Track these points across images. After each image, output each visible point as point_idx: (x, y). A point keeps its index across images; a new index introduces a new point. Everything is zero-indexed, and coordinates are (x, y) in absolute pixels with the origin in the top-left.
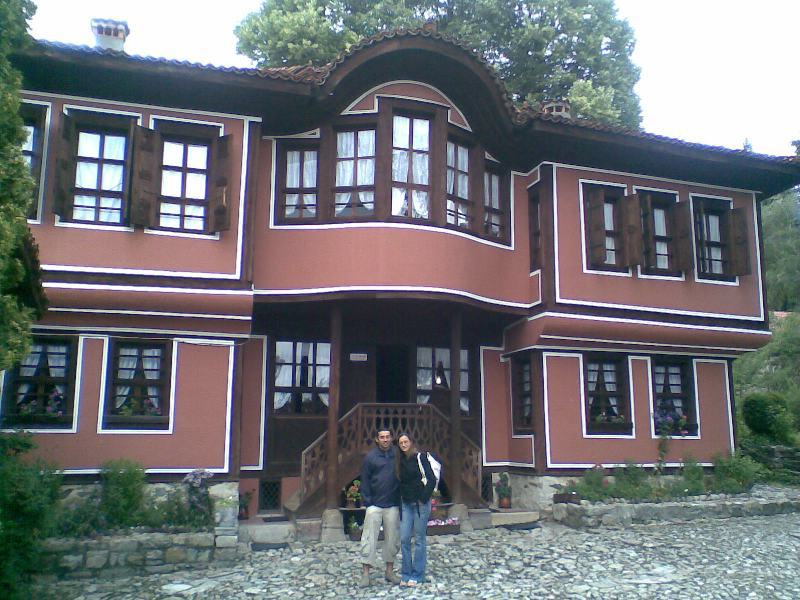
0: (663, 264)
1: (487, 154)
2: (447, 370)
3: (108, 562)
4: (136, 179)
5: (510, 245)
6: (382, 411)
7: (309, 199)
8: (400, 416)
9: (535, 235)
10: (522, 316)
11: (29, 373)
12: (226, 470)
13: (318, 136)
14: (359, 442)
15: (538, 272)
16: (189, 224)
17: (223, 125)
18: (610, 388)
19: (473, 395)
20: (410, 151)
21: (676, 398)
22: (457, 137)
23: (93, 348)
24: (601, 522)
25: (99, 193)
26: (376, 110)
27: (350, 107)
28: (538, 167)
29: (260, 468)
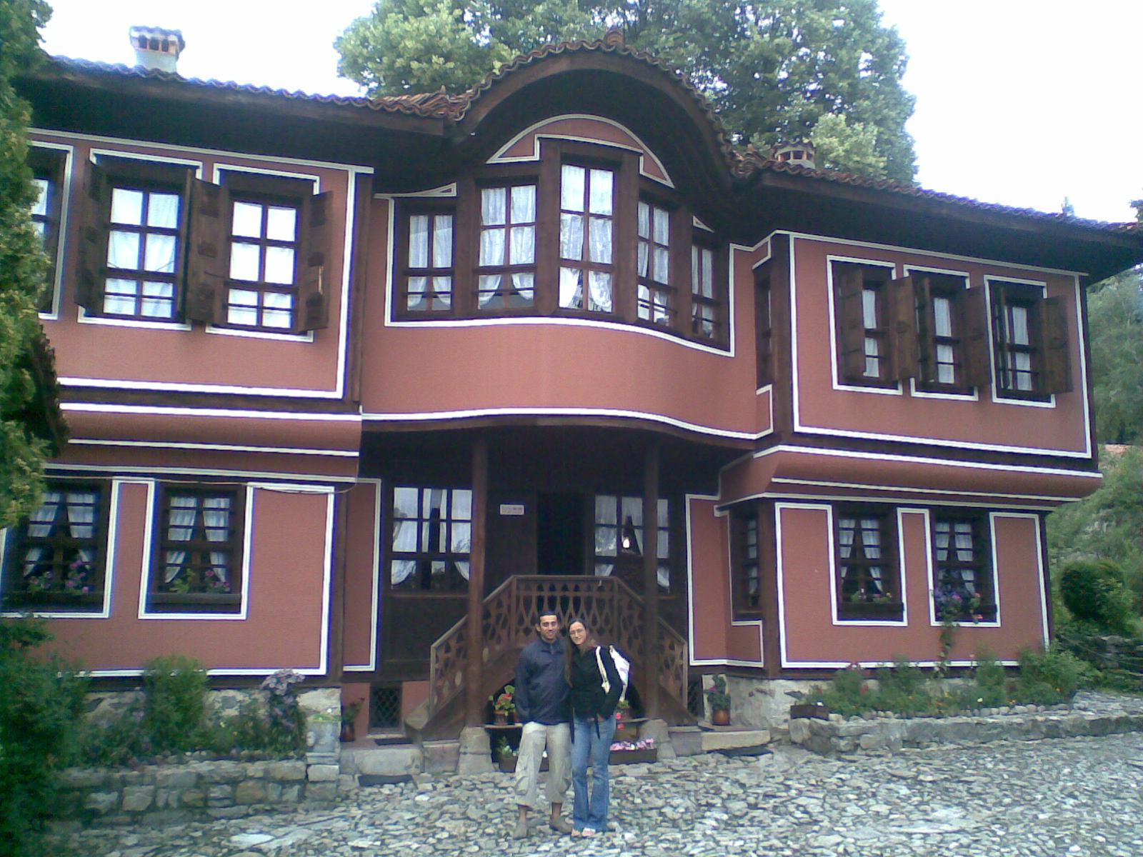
0: (947, 376)
1: (695, 219)
2: (638, 527)
3: (154, 802)
5: (728, 350)
7: (442, 284)
8: (570, 594)
9: (763, 335)
11: (41, 532)
12: (322, 671)
13: (454, 194)
15: (769, 388)
16: (269, 320)
17: (317, 178)
18: (871, 554)
19: (676, 564)
20: (586, 215)
21: (874, 566)
23: (133, 496)
25: (140, 275)
26: (537, 157)
28: (768, 239)
29: (372, 668)
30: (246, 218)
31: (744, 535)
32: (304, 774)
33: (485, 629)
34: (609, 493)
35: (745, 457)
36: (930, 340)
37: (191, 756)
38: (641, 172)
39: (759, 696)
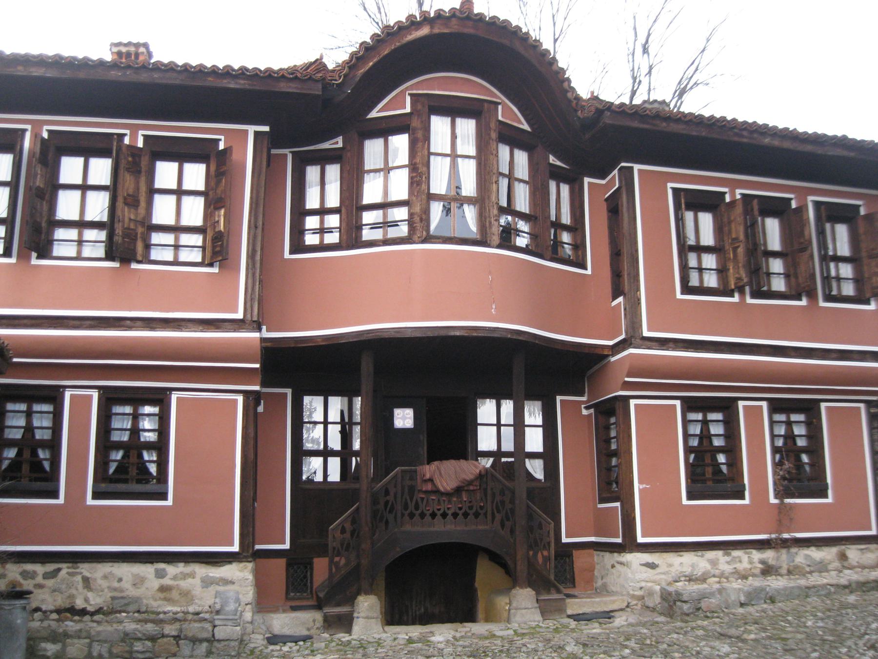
0: (779, 284)
4: (120, 204)
5: (585, 268)
7: (333, 221)
9: (616, 254)
10: (608, 356)
11: (18, 435)
12: (236, 548)
13: (340, 145)
14: (399, 515)
15: (621, 299)
16: (184, 256)
17: (222, 137)
18: (801, 443)
23: (753, 414)
24: (698, 609)
25: (82, 224)
26: (408, 110)
27: (521, 126)
28: (616, 172)
29: (287, 546)
31: (607, 428)
32: (211, 633)
33: (375, 513)
34: (490, 396)
35: (604, 362)
36: (759, 253)
37: (126, 617)
39: (618, 566)
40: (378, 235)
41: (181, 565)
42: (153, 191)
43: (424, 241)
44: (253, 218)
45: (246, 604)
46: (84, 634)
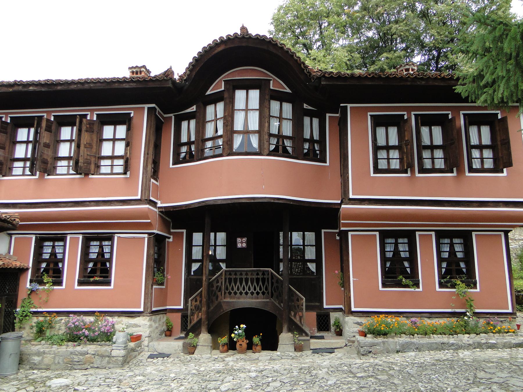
6: (238, 274)
11: (93, 256)
12: (142, 309)
13: (195, 110)
18: (460, 255)
19: (318, 260)
20: (247, 110)
22: (281, 97)
23: (74, 241)
25: (112, 158)
26: (223, 89)
27: (285, 91)
29: (181, 307)
30: (108, 131)
38: (271, 88)
40: (211, 153)
41: (116, 317)
42: (102, 140)
43: (229, 155)
44: (146, 150)
45: (146, 337)
46: (52, 352)
